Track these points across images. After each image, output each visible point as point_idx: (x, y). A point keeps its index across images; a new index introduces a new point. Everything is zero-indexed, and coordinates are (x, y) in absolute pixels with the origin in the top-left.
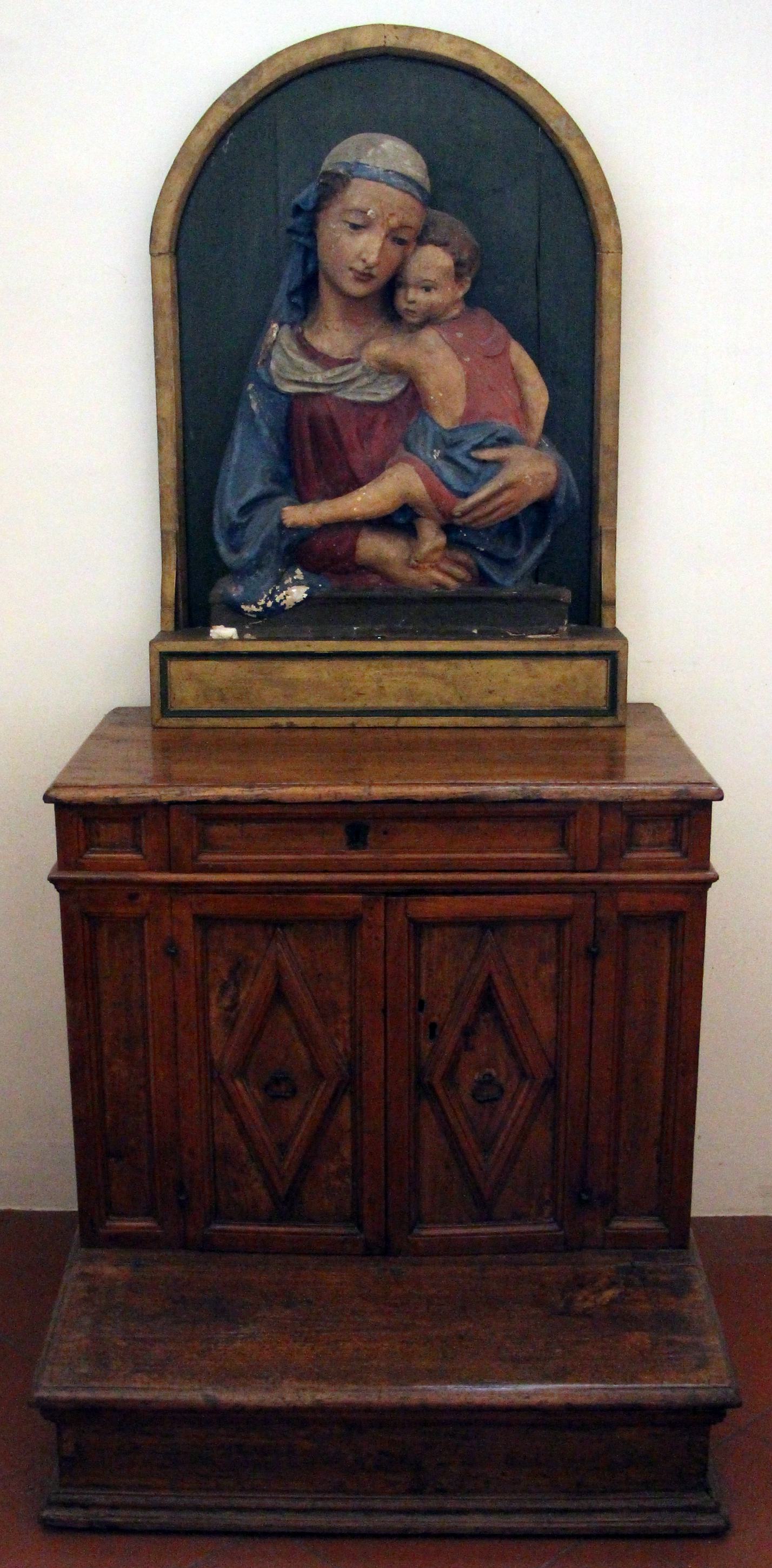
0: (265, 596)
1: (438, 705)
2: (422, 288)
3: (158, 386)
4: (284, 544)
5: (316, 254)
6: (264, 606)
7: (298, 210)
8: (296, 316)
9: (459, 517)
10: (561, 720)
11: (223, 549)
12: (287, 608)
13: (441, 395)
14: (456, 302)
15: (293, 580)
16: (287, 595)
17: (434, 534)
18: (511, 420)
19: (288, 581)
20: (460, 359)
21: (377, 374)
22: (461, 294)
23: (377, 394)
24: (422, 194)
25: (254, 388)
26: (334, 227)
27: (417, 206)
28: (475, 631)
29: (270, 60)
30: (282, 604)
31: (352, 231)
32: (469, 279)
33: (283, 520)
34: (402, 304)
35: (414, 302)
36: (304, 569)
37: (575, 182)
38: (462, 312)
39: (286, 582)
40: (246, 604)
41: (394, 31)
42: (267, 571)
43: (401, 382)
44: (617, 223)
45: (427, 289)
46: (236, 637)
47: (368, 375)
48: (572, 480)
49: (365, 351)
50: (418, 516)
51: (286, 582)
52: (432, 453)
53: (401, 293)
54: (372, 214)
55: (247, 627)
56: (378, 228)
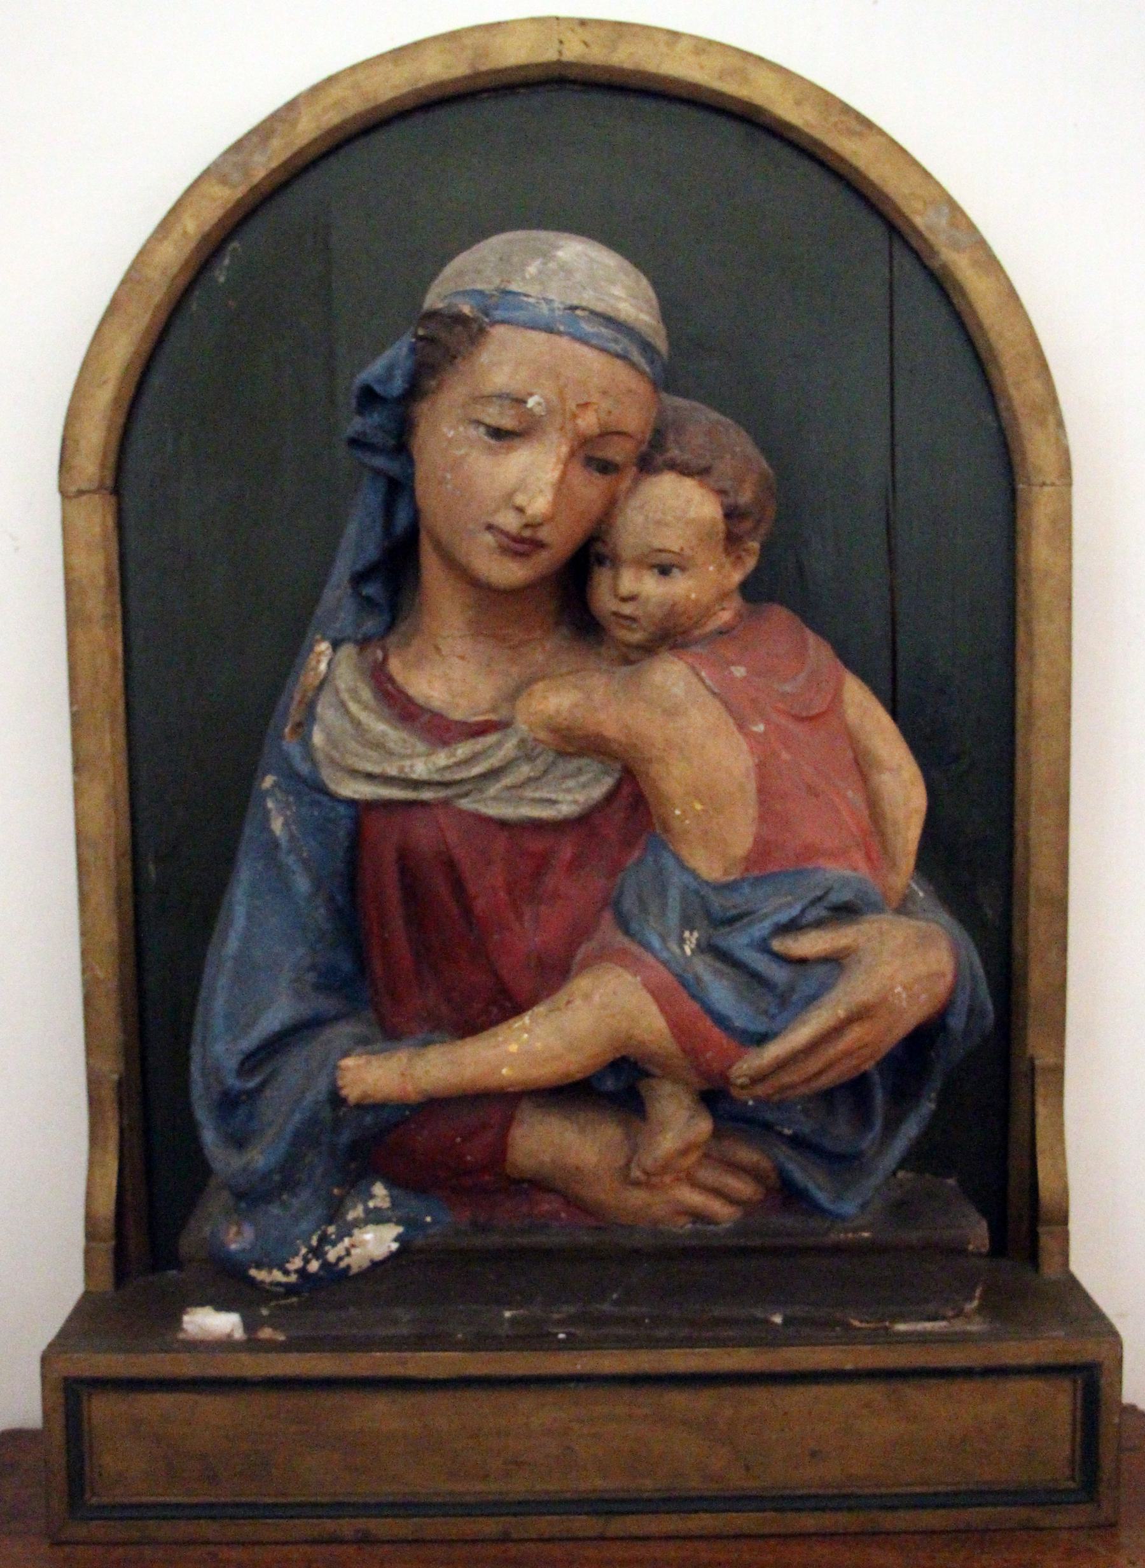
0: (304, 1251)
1: (694, 1484)
2: (652, 567)
3: (77, 769)
4: (345, 1137)
5: (413, 491)
6: (302, 1272)
7: (369, 397)
8: (371, 625)
9: (742, 1087)
10: (975, 1516)
11: (209, 1137)
12: (355, 1270)
13: (698, 807)
14: (724, 596)
15: (367, 1211)
16: (353, 1246)
17: (684, 1114)
18: (858, 857)
19: (356, 1212)
20: (741, 727)
21: (550, 756)
22: (737, 577)
23: (553, 802)
24: (651, 362)
25: (276, 785)
26: (451, 434)
27: (641, 387)
28: (778, 1319)
29: (316, 90)
30: (342, 1265)
31: (493, 442)
32: (755, 545)
33: (341, 1088)
34: (604, 600)
35: (631, 598)
36: (392, 1183)
37: (970, 341)
38: (739, 615)
39: (351, 1216)
40: (259, 1266)
41: (579, 30)
42: (305, 1194)
43: (606, 773)
44: (1060, 424)
45: (664, 571)
46: (239, 1334)
47: (529, 758)
48: (981, 972)
49: (521, 704)
50: (648, 1075)
51: (351, 1216)
52: (682, 941)
53: (602, 579)
54: (539, 404)
55: (265, 1312)
56: (554, 436)
